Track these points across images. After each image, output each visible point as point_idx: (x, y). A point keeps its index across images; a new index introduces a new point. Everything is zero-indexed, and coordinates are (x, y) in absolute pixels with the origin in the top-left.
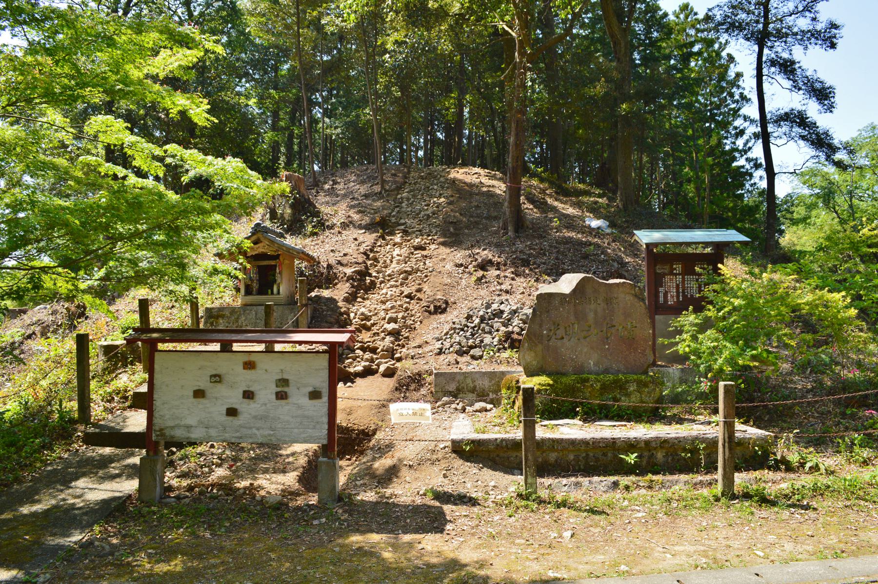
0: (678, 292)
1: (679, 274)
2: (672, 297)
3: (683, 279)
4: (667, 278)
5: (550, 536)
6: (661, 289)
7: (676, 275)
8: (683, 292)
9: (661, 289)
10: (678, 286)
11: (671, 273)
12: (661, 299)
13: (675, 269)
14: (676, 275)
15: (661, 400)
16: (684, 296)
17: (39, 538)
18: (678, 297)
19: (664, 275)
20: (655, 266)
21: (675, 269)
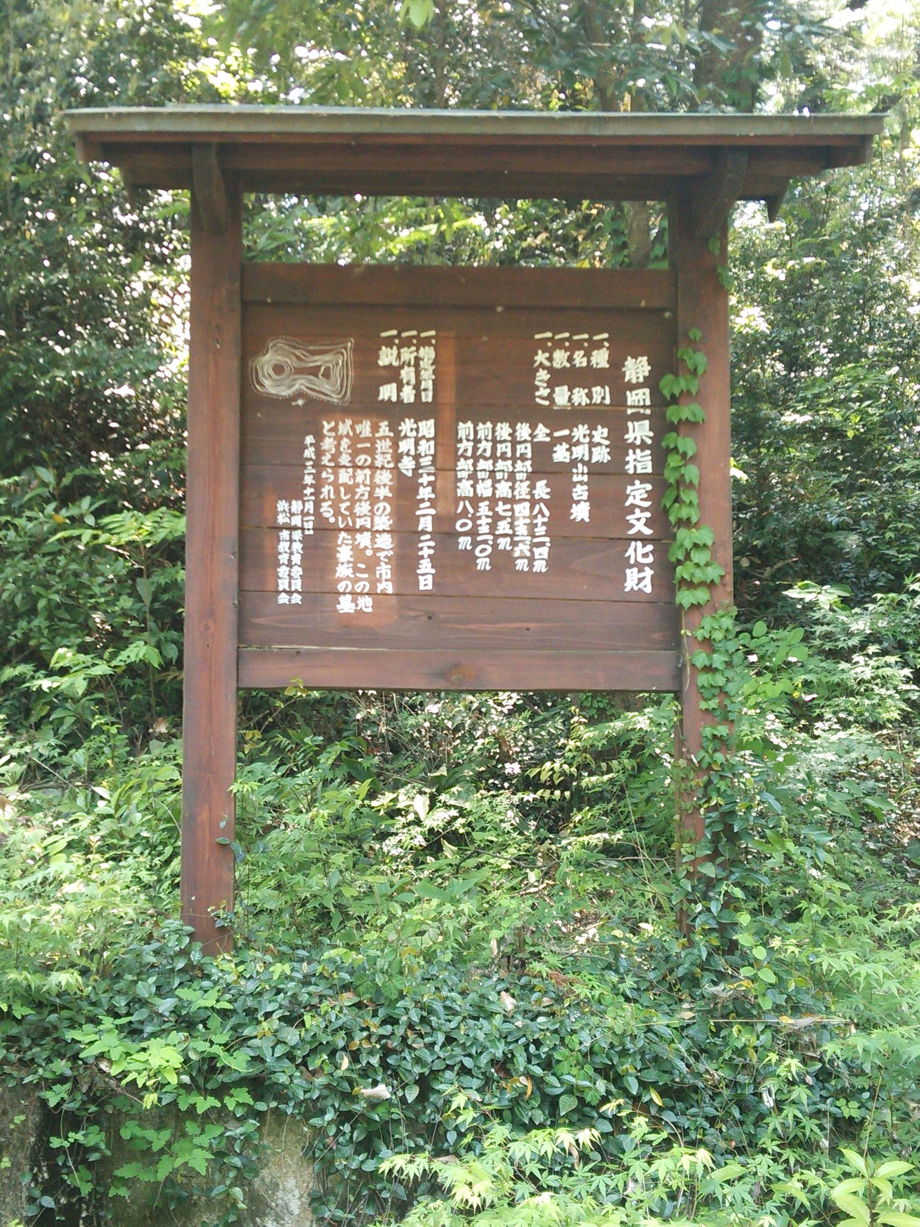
0: (405, 532)
1: (418, 411)
2: (366, 563)
3: (446, 440)
4: (336, 435)
5: (797, 471)
6: (289, 511)
7: (395, 412)
8: (445, 533)
9: (289, 511)
10: (405, 489)
11: (364, 404)
12: (289, 578)
13: (393, 375)
14: (395, 412)
15: (676, 449)
16: (452, 560)
17: (424, 849)
18: (405, 563)
19: (317, 411)
20: (249, 348)
21: (393, 375)
